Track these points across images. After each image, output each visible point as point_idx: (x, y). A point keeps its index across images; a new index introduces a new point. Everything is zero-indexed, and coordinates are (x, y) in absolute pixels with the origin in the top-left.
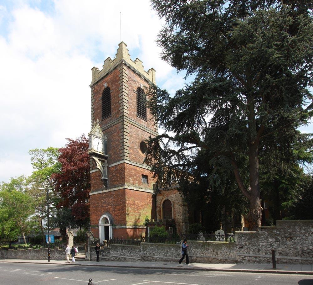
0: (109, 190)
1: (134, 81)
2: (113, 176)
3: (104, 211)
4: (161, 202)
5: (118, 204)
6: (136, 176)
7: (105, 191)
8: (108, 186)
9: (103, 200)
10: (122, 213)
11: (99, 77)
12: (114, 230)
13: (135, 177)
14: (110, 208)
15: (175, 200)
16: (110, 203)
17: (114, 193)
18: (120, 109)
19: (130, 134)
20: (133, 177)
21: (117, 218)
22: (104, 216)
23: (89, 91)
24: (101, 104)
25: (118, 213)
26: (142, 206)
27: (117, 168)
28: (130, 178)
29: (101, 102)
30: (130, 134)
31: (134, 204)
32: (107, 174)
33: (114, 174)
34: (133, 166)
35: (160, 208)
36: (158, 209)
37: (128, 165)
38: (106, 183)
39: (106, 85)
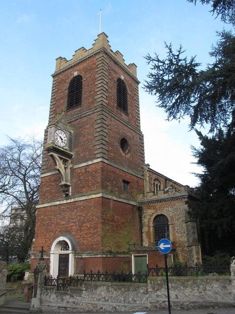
0: (72, 200)
1: (115, 71)
2: (80, 180)
3: (60, 232)
4: (149, 219)
5: (87, 219)
6: (116, 181)
7: (65, 202)
8: (70, 194)
9: (60, 214)
10: (94, 234)
11: (64, 65)
12: (77, 261)
13: (114, 182)
14: (72, 226)
15: (173, 214)
16: (73, 219)
17: (81, 204)
18: (95, 98)
19: (110, 127)
20: (112, 182)
21: (85, 242)
22: (61, 238)
23: (50, 81)
24: (67, 94)
25: (86, 234)
26: (123, 224)
27: (87, 170)
28: (108, 183)
29: (67, 92)
30: (110, 127)
31: (113, 221)
32: (69, 178)
33: (82, 178)
34: (112, 167)
35: (149, 227)
36: (145, 229)
37: (106, 165)
38: (68, 191)
39: (76, 74)
